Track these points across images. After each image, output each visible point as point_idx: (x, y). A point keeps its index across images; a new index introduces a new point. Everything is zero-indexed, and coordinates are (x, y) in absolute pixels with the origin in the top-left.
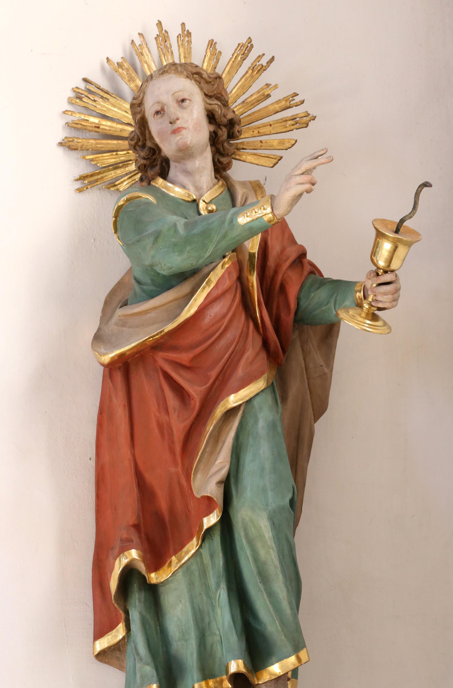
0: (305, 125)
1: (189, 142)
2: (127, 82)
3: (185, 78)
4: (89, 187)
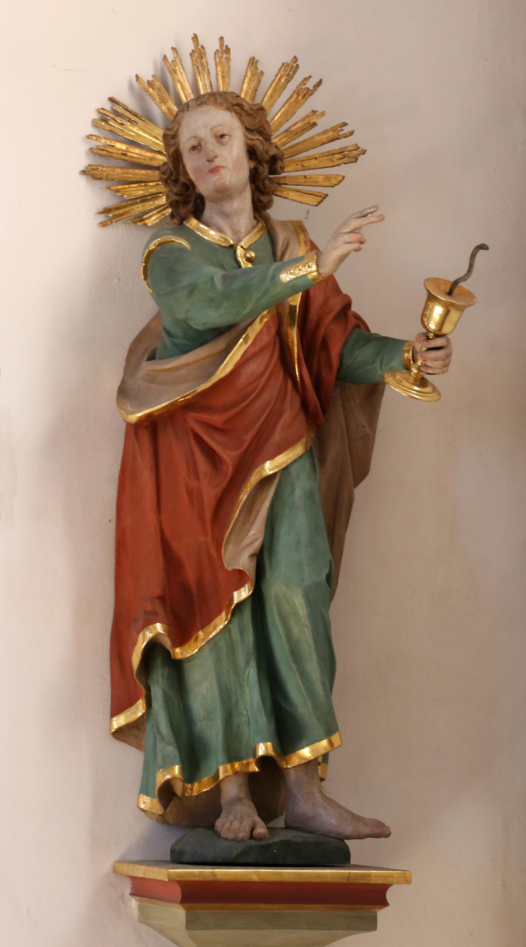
0: (353, 160)
1: (227, 183)
2: (158, 104)
3: (225, 110)
4: (114, 221)
